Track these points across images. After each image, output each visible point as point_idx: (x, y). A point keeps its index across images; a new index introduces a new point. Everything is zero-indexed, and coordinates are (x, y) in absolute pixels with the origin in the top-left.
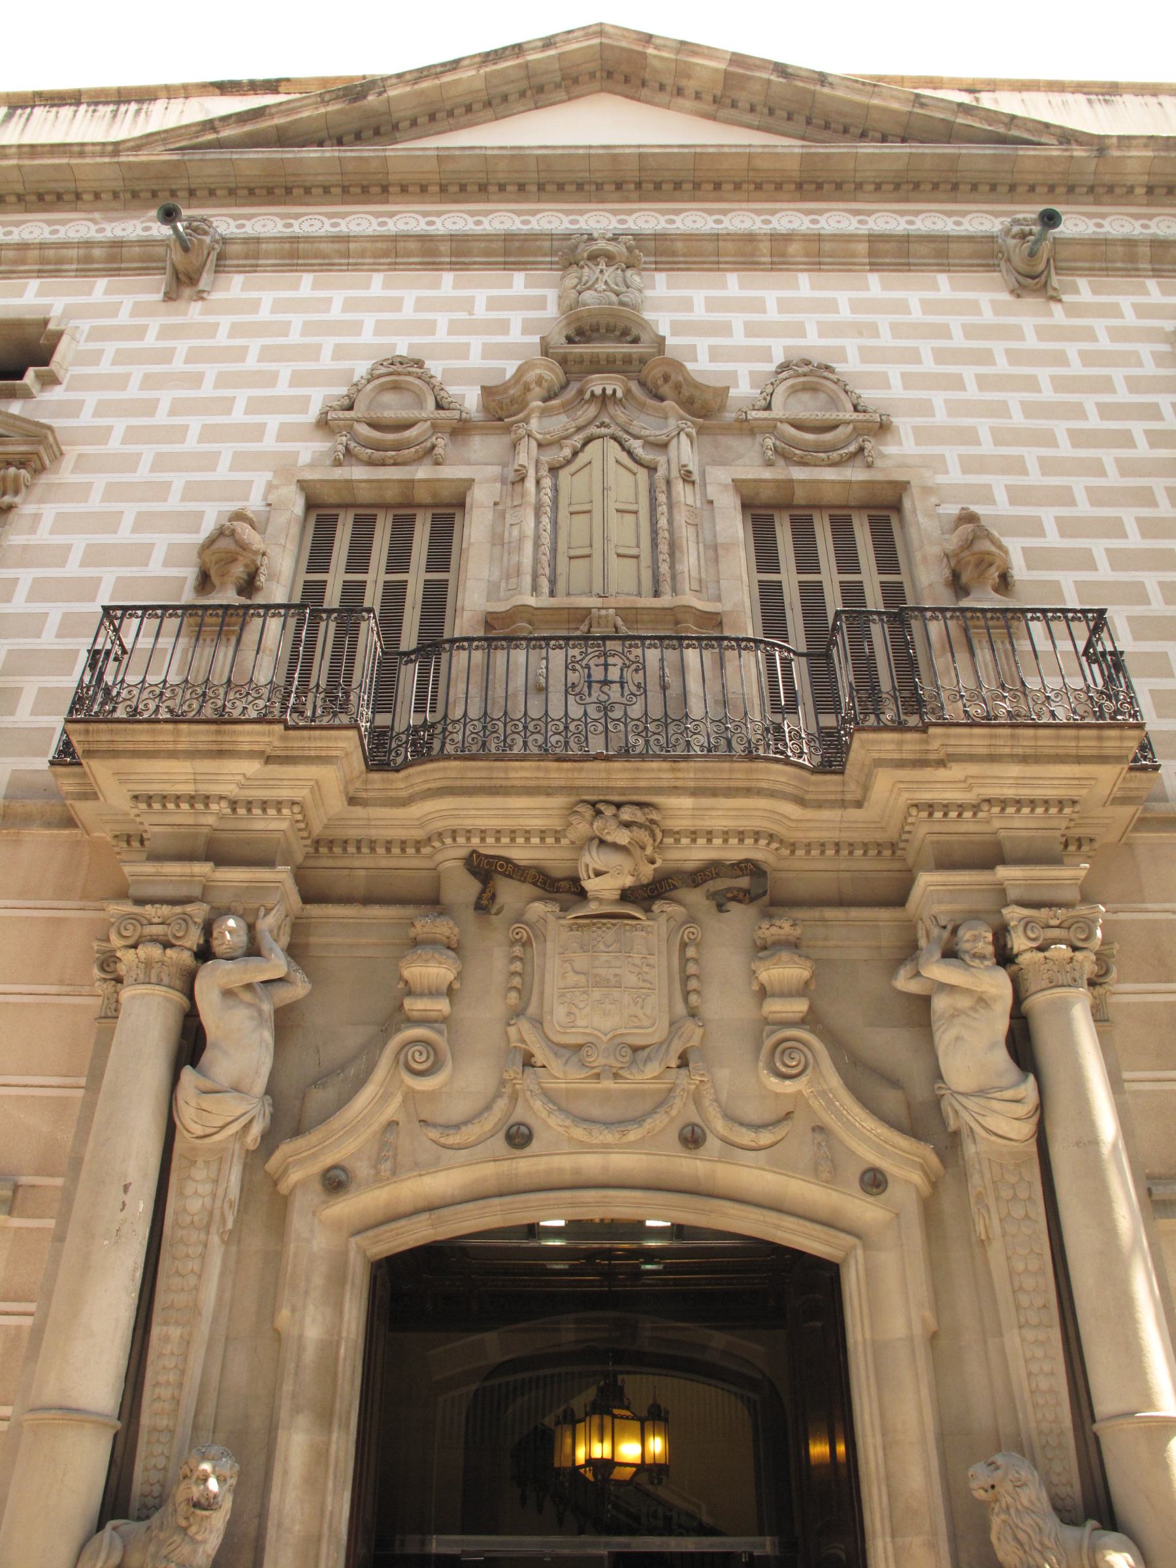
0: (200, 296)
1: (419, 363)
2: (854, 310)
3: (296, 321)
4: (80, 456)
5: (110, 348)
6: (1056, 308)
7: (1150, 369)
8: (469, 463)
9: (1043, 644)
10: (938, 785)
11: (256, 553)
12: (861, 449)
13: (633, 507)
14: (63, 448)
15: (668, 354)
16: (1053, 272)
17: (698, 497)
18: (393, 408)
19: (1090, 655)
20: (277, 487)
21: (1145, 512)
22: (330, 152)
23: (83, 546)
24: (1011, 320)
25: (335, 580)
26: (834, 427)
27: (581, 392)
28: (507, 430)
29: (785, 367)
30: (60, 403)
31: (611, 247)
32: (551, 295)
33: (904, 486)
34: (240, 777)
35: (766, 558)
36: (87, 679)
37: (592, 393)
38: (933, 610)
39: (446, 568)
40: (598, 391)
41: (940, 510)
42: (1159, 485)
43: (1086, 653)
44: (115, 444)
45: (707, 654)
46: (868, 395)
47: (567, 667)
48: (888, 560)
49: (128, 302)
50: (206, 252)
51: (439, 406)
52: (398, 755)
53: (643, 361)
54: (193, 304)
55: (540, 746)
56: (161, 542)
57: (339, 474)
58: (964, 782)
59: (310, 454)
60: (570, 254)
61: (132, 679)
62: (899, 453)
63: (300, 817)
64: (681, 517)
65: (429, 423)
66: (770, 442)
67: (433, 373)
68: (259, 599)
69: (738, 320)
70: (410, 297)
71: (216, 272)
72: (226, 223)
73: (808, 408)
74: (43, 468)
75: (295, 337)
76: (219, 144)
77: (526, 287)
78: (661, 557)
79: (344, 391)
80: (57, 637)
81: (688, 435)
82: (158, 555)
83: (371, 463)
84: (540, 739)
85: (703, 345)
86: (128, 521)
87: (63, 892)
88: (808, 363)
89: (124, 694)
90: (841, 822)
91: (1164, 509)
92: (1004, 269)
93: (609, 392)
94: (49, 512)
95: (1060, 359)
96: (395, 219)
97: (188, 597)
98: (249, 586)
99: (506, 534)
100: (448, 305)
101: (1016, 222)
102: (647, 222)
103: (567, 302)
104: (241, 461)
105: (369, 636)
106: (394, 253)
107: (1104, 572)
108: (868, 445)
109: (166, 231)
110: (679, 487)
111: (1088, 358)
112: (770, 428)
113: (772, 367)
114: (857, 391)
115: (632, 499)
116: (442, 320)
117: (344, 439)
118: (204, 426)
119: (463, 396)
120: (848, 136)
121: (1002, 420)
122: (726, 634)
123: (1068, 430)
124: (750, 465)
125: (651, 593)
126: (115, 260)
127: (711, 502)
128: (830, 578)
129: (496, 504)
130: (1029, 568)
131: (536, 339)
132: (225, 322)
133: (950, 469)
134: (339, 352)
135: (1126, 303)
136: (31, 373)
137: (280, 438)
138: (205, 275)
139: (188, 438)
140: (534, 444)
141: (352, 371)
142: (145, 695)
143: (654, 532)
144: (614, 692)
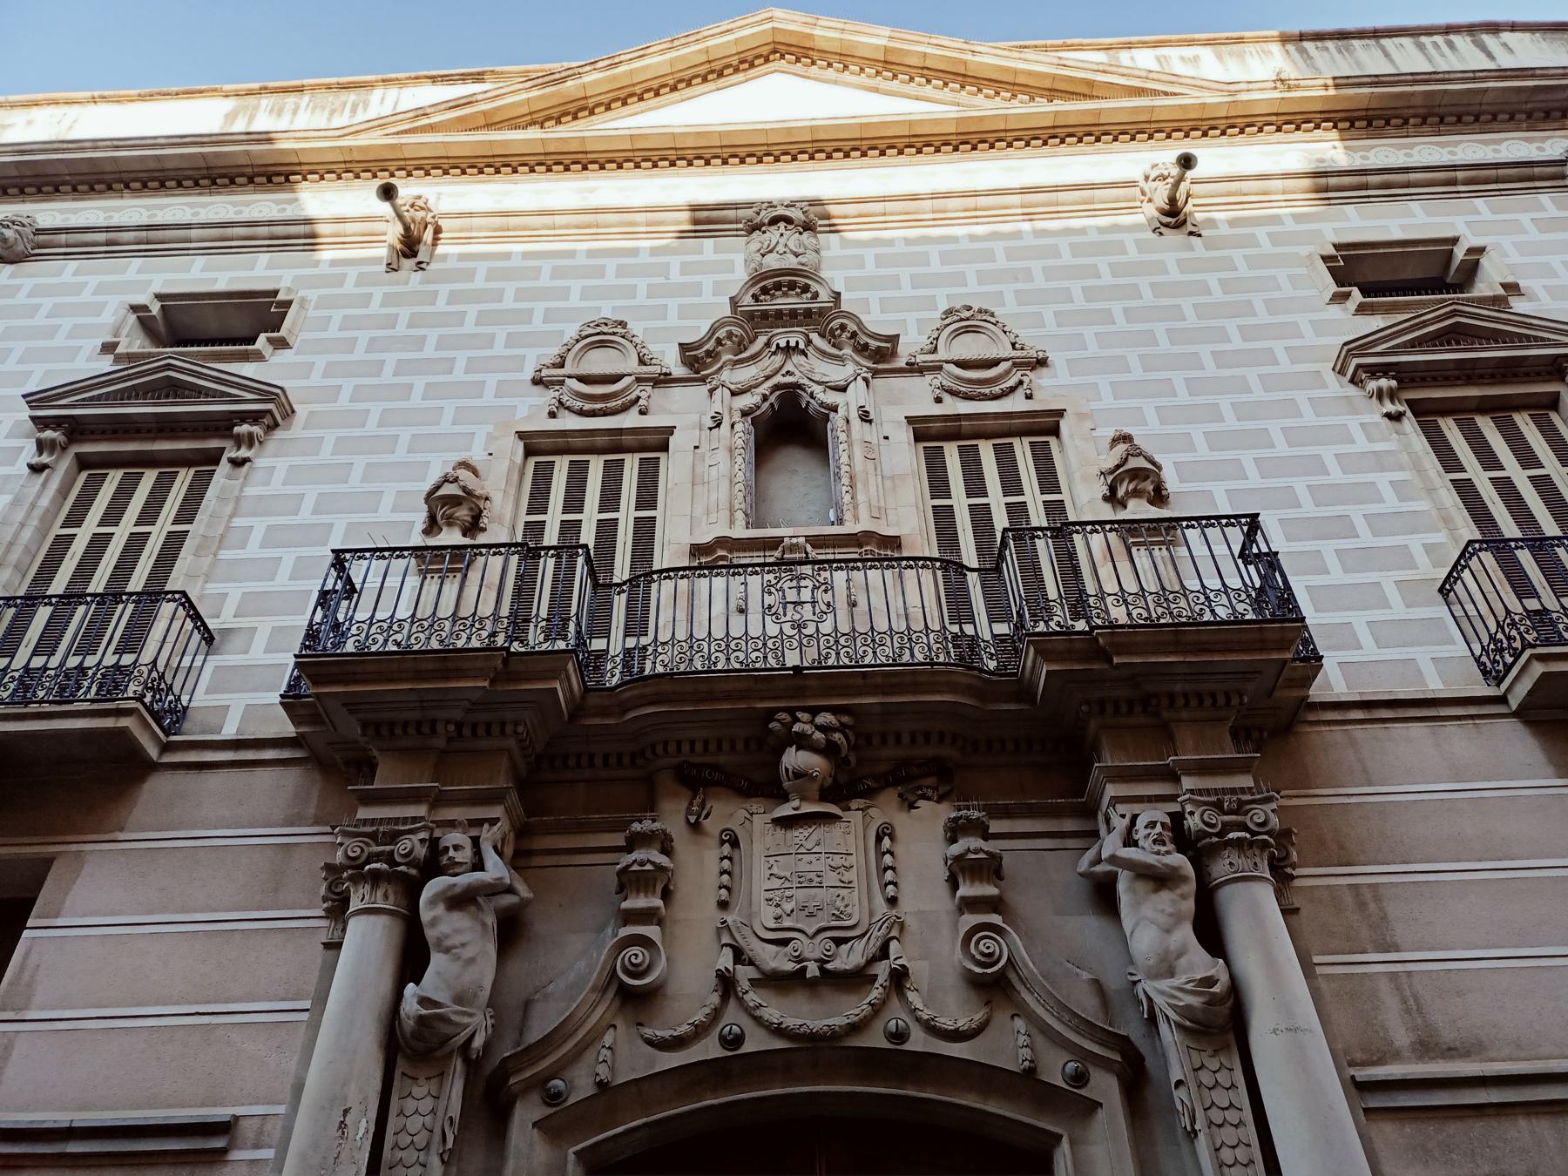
1: (623, 324)
9: (1200, 550)
11: (478, 498)
18: (600, 362)
22: (534, 133)
25: (554, 517)
26: (995, 363)
27: (768, 344)
28: (703, 380)
29: (949, 312)
31: (788, 213)
32: (739, 259)
33: (1060, 413)
34: (466, 704)
35: (939, 484)
36: (318, 617)
38: (1093, 523)
40: (783, 344)
45: (888, 573)
46: (1026, 336)
48: (1049, 481)
51: (642, 362)
53: (822, 312)
57: (554, 425)
59: (533, 411)
61: (362, 615)
62: (1047, 390)
66: (937, 383)
68: (482, 539)
74: (277, 425)
76: (432, 128)
81: (865, 379)
83: (582, 413)
84: (742, 656)
85: (874, 297)
88: (969, 308)
89: (354, 630)
93: (793, 344)
94: (282, 465)
97: (417, 540)
98: (473, 526)
107: (1254, 480)
109: (385, 208)
113: (938, 314)
122: (905, 554)
124: (919, 397)
128: (996, 500)
132: (444, 290)
134: (549, 316)
136: (262, 337)
141: (562, 333)
142: (373, 630)
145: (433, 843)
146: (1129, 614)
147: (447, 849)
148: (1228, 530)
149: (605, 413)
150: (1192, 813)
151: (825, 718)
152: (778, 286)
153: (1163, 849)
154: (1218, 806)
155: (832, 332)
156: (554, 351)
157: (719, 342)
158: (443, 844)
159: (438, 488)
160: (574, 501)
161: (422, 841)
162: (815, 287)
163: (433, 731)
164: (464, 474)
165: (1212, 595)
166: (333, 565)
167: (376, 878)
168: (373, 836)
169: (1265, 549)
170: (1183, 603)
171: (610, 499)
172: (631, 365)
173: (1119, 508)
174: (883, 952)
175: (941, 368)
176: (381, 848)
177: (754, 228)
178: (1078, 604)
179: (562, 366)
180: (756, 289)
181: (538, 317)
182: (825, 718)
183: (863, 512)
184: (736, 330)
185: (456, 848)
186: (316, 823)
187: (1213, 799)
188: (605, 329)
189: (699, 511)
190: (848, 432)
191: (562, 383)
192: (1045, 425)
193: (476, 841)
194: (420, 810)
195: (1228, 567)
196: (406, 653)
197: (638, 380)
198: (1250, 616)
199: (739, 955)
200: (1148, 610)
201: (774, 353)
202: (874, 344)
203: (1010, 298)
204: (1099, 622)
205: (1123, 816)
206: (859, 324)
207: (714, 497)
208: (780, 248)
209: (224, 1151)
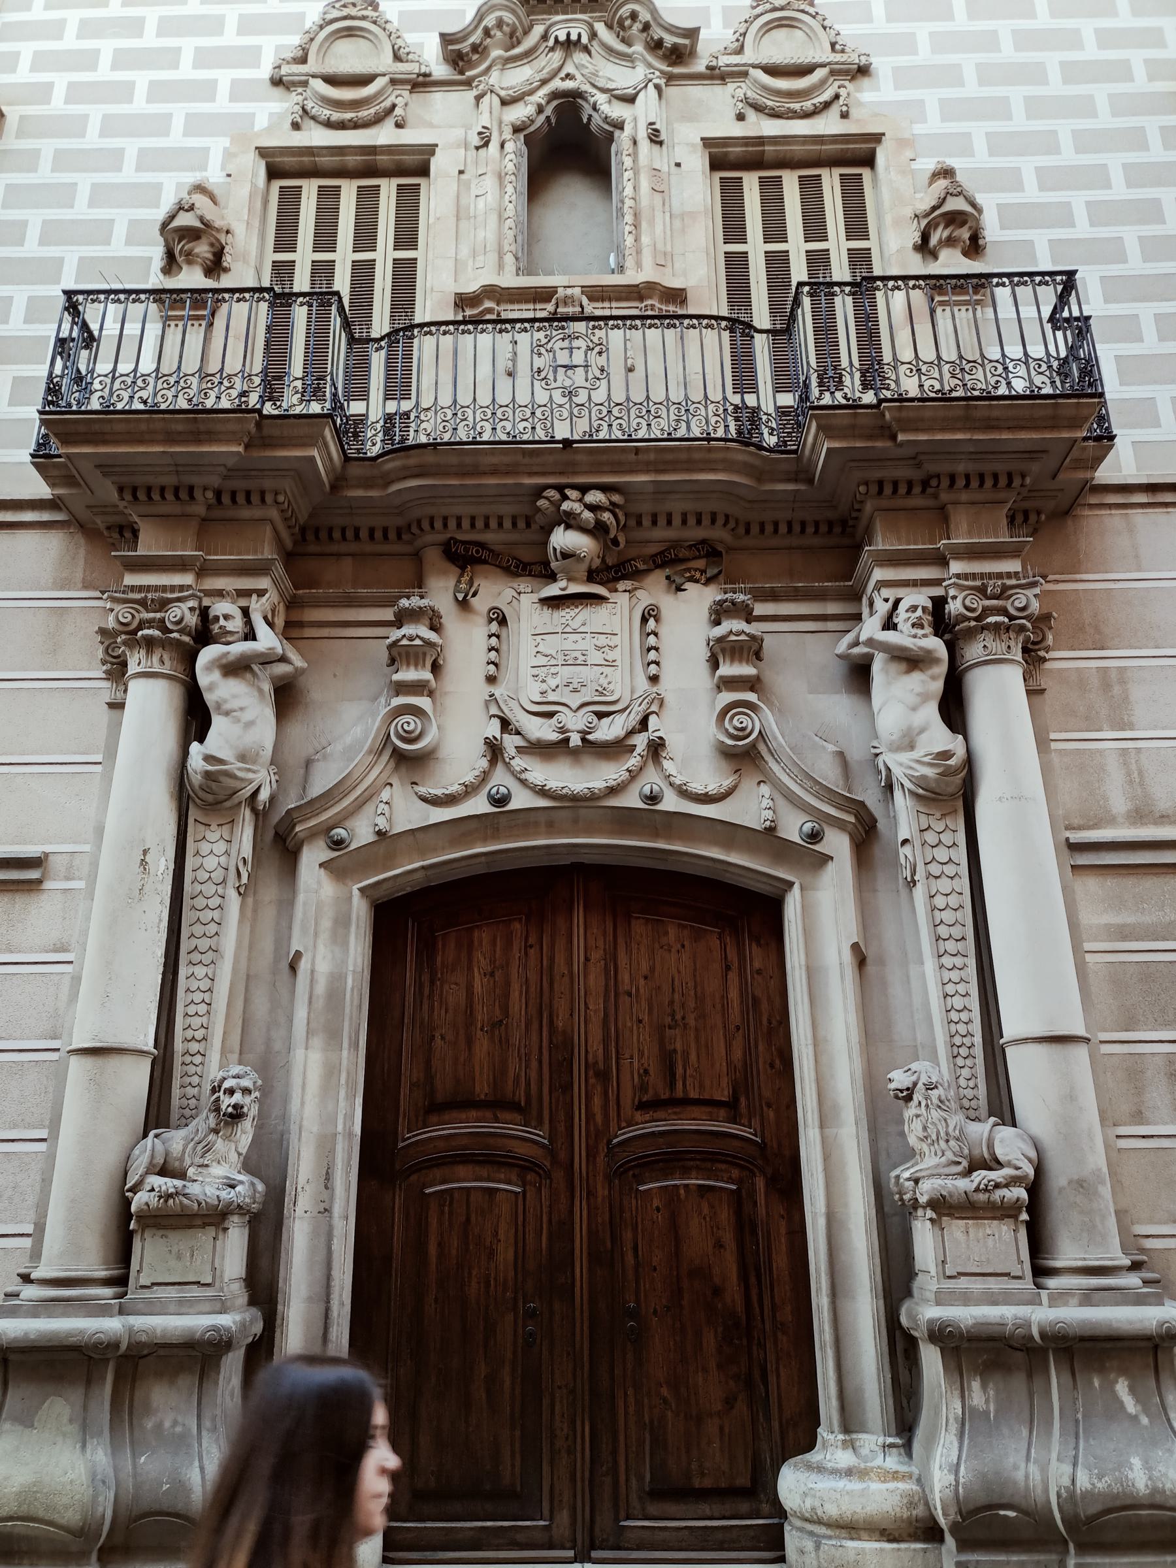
4: (22, 118)
8: (431, 125)
10: (889, 463)
11: (218, 230)
18: (349, 57)
20: (234, 155)
27: (545, 37)
28: (468, 83)
33: (877, 138)
34: (222, 469)
36: (58, 369)
37: (556, 38)
39: (414, 247)
40: (562, 37)
41: (914, 165)
42: (1152, 124)
43: (1051, 319)
44: (58, 103)
46: (848, 31)
47: (532, 351)
48: (857, 226)
51: (397, 58)
52: (374, 445)
55: (508, 433)
56: (121, 218)
58: (914, 458)
59: (271, 120)
62: (869, 106)
66: (740, 93)
67: (388, 17)
68: (226, 282)
79: (295, 40)
80: (25, 322)
81: (657, 87)
82: (120, 231)
83: (329, 124)
90: (794, 501)
93: (574, 37)
97: (155, 280)
98: (215, 266)
99: (472, 206)
104: (195, 125)
107: (1082, 229)
108: (843, 92)
110: (644, 145)
112: (741, 74)
114: (836, 27)
117: (300, 98)
119: (421, 45)
121: (992, 55)
124: (718, 113)
127: (678, 165)
128: (797, 246)
139: (136, 98)
141: (302, 16)
144: (579, 376)
145: (204, 612)
146: (921, 386)
147: (217, 619)
149: (356, 125)
150: (954, 598)
151: (594, 497)
153: (920, 632)
154: (982, 591)
158: (212, 613)
159: (172, 217)
161: (191, 609)
164: (200, 200)
167: (150, 644)
168: (143, 603)
170: (980, 375)
173: (930, 259)
174: (644, 724)
175: (745, 74)
176: (152, 615)
178: (872, 371)
179: (303, 60)
182: (594, 497)
183: (647, 259)
184: (508, 17)
186: (86, 587)
187: (978, 583)
188: (353, 12)
189: (465, 251)
190: (635, 156)
191: (305, 84)
192: (858, 155)
193: (245, 612)
194: (187, 579)
195: (1032, 332)
199: (505, 724)
200: (941, 381)
201: (552, 49)
202: (670, 40)
205: (886, 600)
207: (481, 234)
209: (39, 882)
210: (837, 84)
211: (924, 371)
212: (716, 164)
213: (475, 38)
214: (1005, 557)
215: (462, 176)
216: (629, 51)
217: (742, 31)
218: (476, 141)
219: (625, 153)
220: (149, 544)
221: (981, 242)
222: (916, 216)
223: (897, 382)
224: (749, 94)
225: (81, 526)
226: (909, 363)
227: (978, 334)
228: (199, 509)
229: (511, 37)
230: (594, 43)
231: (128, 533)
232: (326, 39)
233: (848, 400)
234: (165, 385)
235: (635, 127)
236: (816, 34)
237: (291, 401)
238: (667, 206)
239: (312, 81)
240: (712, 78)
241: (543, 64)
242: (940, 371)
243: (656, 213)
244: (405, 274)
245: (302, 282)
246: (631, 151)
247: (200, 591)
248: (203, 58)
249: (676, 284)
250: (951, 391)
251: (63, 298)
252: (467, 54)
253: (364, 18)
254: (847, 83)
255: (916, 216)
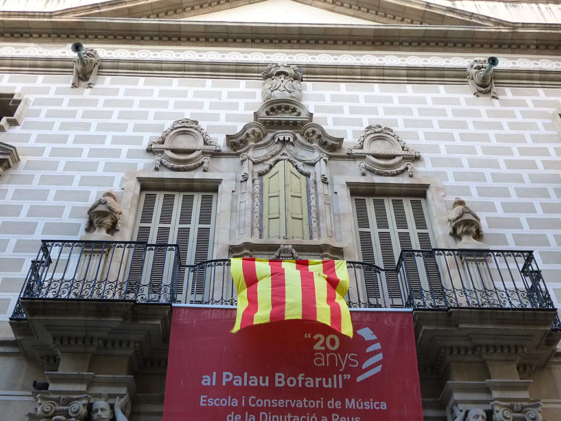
0: (90, 86)
1: (196, 122)
2: (401, 102)
3: (137, 100)
5: (44, 109)
6: (495, 101)
7: (542, 131)
8: (220, 171)
9: (503, 266)
11: (116, 213)
12: (407, 168)
13: (299, 195)
14: (20, 157)
15: (314, 121)
16: (494, 85)
17: (330, 190)
18: (183, 143)
19: (525, 272)
20: (127, 180)
21: (544, 200)
23: (28, 206)
24: (475, 108)
27: (273, 138)
28: (238, 155)
29: (369, 128)
30: (19, 134)
32: (259, 92)
33: (427, 186)
35: (363, 221)
37: (279, 139)
41: (445, 198)
42: (550, 187)
46: (409, 143)
48: (421, 222)
49: (54, 87)
50: (93, 65)
51: (205, 143)
53: (302, 123)
54: (86, 89)
55: (100, 294)
56: (68, 206)
57: (157, 175)
59: (145, 166)
60: (268, 73)
62: (422, 173)
63: (138, 349)
64: (321, 201)
65: (201, 151)
66: (363, 164)
68: (117, 237)
69: (346, 106)
70: (191, 90)
71: (98, 75)
72: (104, 51)
73: (380, 148)
74: (9, 167)
75: (136, 108)
76: (100, 15)
77: (246, 87)
78: (313, 219)
79: (160, 135)
81: (325, 160)
82: (67, 212)
83: (173, 169)
86: (52, 194)
87: (11, 387)
88: (380, 127)
91: (554, 199)
92: (470, 84)
93: (287, 139)
95: (499, 126)
96: (184, 53)
97: (81, 235)
98: (112, 229)
99: (238, 207)
100: (209, 95)
101: (476, 61)
102: (302, 58)
103: (266, 96)
104: (109, 167)
105: (170, 256)
106: (183, 69)
107: (526, 230)
108: (409, 167)
109: (75, 55)
110: (320, 185)
111: (512, 126)
112: (362, 157)
113: (363, 128)
115: (299, 191)
116: (206, 102)
117: (160, 158)
118: (91, 149)
120: (395, 21)
123: (505, 160)
124: (354, 173)
125: (309, 237)
126: (48, 66)
127: (336, 193)
128: (393, 230)
129: (233, 191)
130: (490, 227)
131: (252, 113)
132: (102, 99)
133: (449, 178)
134: (157, 116)
135: (529, 100)
137: (128, 156)
138: (92, 76)
140: (251, 163)
141: (163, 125)
143: (309, 207)
145: (90, 407)
146: (468, 302)
147: (97, 410)
148: (517, 258)
149: (184, 170)
150: (498, 411)
152: (279, 108)
154: (511, 408)
155: (308, 134)
156: (159, 135)
157: (248, 135)
158: (94, 407)
159: (95, 206)
160: (166, 217)
161: (84, 405)
162: (299, 109)
163: (91, 342)
164: (109, 200)
165: (510, 294)
166: (42, 248)
168: (58, 401)
169: (535, 268)
170: (495, 297)
171: (186, 217)
172: (200, 145)
173: (458, 240)
175: (365, 157)
176: (62, 408)
177: (267, 76)
178: (438, 291)
179: (163, 143)
180: (268, 109)
181: (151, 116)
183: (323, 233)
184: (257, 130)
185: (102, 410)
186: (23, 389)
187: (508, 404)
188: (187, 125)
189: (234, 226)
190: (316, 188)
191: (162, 152)
192: (419, 193)
193: (112, 407)
194: (83, 388)
195: (517, 276)
196: (79, 300)
197: (204, 153)
198: (529, 306)
200: (477, 299)
201: (277, 143)
202: (330, 142)
203: (401, 123)
204: (452, 305)
205: (461, 411)
206: (323, 131)
207: (243, 219)
208: (282, 88)
210: (406, 164)
211: (468, 294)
212: (353, 193)
213: (243, 137)
214: (520, 390)
215: (234, 193)
216: (313, 145)
217: (362, 140)
218: (241, 179)
219: (311, 187)
220: (66, 367)
221: (481, 233)
222: (449, 220)
223: (456, 299)
224: (367, 165)
225: (26, 355)
226: (461, 290)
227: (491, 277)
228: (93, 350)
229: (258, 137)
230: (296, 142)
231: (52, 361)
232: (173, 135)
233: (432, 306)
234: (88, 287)
235: (316, 177)
236: (395, 143)
237: (144, 295)
238: (331, 211)
239: (165, 151)
240: (349, 158)
241: (273, 149)
242: (476, 294)
243: (327, 213)
244: (204, 236)
245: (153, 239)
246: (314, 186)
247: (90, 394)
248: (115, 140)
249: (337, 245)
250: (483, 305)
251: (41, 243)
252: (238, 143)
253: (191, 127)
254: (410, 163)
255: (449, 220)
